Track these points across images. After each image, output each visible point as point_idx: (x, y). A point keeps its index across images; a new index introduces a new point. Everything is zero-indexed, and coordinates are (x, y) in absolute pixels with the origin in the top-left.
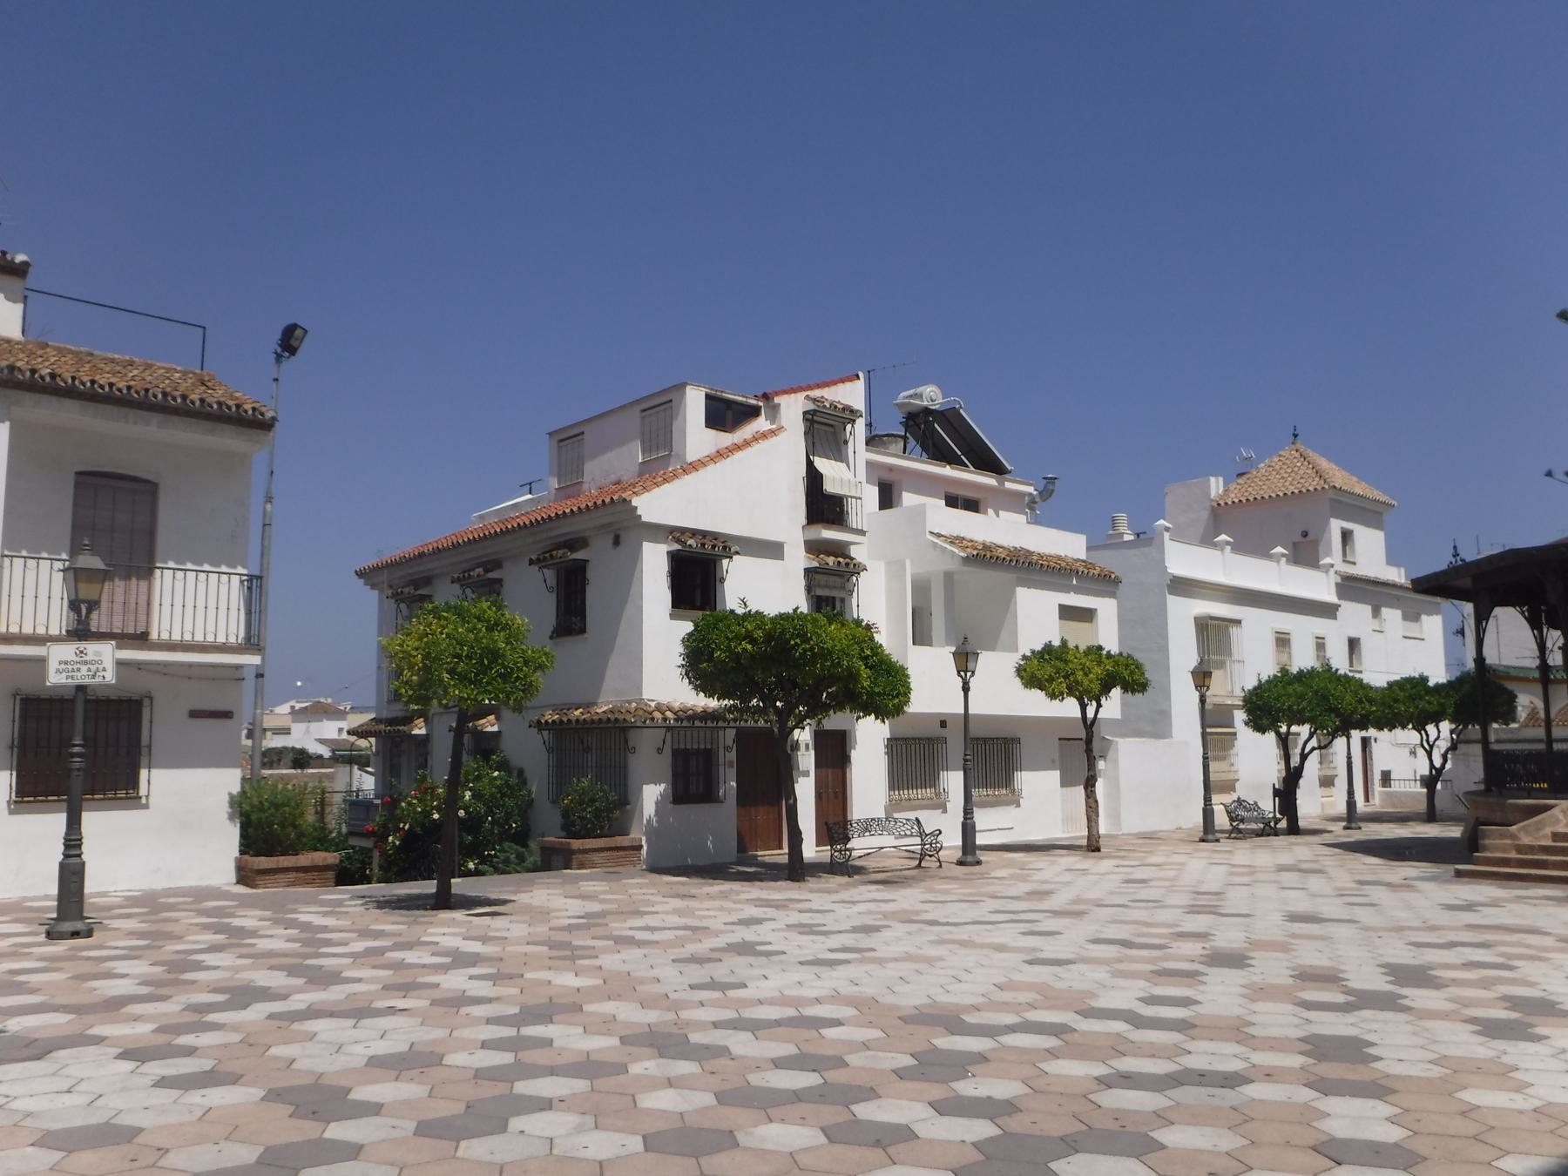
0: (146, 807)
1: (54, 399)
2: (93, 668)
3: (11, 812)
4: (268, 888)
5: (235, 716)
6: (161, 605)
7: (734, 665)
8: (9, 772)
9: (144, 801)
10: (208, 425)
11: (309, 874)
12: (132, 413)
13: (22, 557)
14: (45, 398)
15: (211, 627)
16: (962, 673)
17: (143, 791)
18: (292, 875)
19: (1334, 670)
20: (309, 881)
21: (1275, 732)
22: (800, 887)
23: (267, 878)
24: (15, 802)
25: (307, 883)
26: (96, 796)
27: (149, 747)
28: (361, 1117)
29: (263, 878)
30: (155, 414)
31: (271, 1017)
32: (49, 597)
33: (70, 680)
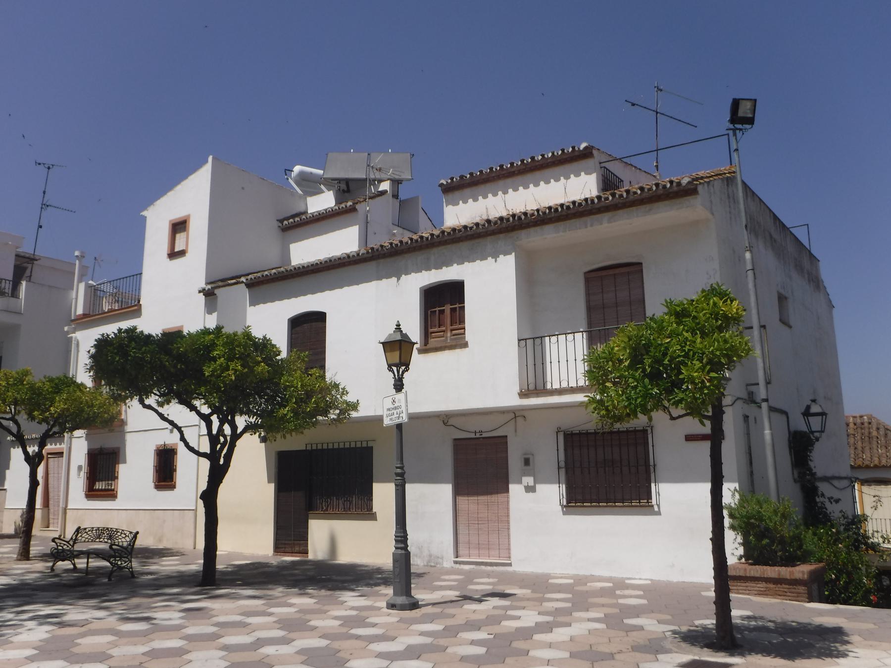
0: (659, 513)
1: (538, 229)
2: (398, 411)
3: (564, 513)
4: (741, 593)
5: (171, 434)
6: (551, 362)
7: (664, 362)
8: (558, 485)
9: (656, 508)
10: (643, 208)
11: (779, 586)
12: (588, 219)
13: (556, 335)
14: (532, 230)
15: (564, 376)
16: (395, 369)
17: (654, 501)
18: (762, 585)
19: (96, 343)
20: (780, 593)
21: (211, 413)
22: (524, 595)
23: (739, 584)
24: (565, 506)
25: (775, 595)
26: (616, 504)
27: (559, 468)
28: (99, 635)
29: (735, 584)
30: (603, 214)
31: (393, 639)
32: (567, 361)
33: (391, 422)
